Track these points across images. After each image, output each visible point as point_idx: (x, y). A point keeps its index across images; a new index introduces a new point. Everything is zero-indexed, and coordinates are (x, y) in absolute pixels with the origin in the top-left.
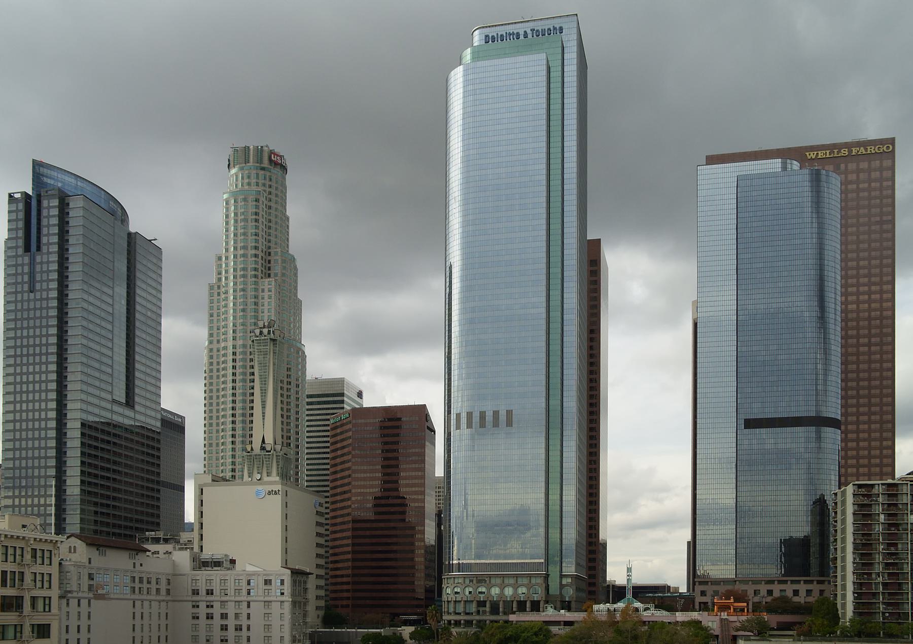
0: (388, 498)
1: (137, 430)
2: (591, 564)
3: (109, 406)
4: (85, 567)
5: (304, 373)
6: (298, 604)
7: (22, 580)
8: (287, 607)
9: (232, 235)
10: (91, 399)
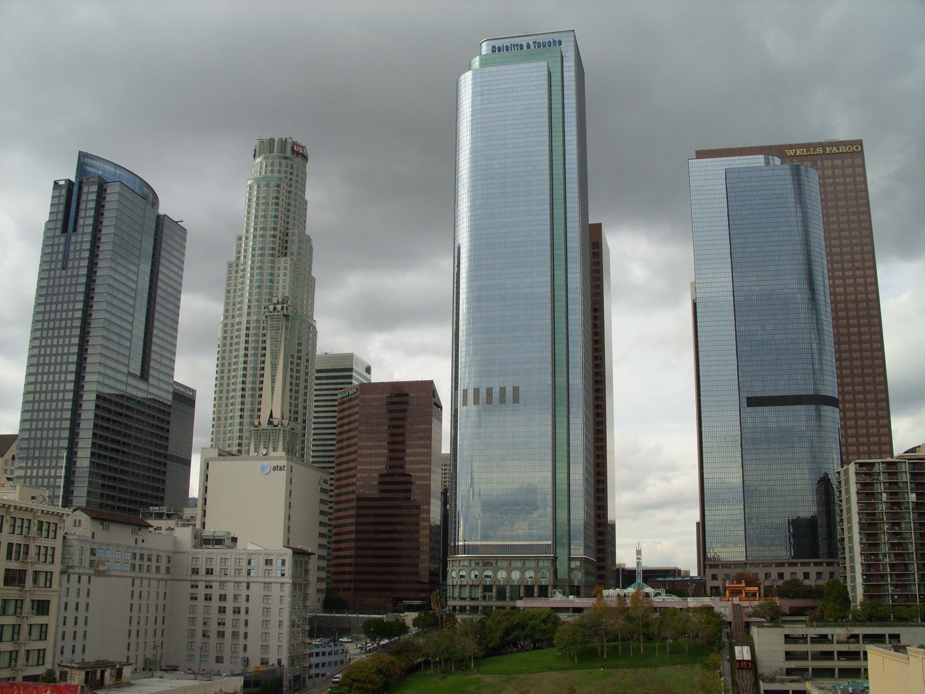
0: (393, 475)
1: (149, 403)
2: (601, 547)
3: (124, 379)
4: (88, 542)
5: (314, 348)
6: (299, 586)
7: (27, 553)
8: (287, 589)
9: (253, 217)
10: (108, 372)
